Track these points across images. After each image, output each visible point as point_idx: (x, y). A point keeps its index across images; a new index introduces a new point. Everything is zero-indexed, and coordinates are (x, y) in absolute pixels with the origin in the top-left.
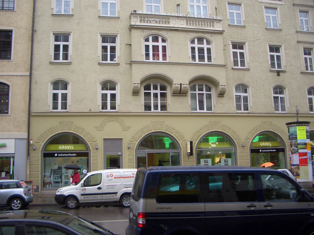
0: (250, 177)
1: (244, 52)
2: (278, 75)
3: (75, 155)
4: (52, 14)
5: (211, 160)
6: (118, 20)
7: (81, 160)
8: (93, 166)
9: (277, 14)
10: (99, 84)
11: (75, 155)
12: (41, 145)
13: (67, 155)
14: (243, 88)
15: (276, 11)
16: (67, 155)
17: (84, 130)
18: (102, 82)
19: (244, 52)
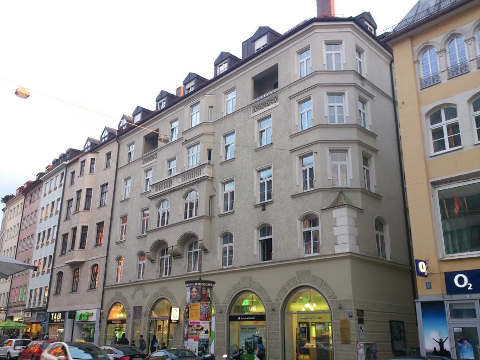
0: (154, 346)
1: (441, 122)
2: (264, 210)
3: (254, 318)
4: (221, 163)
5: (233, 322)
6: (272, 147)
7: (362, 311)
8: (278, 330)
9: (345, 102)
10: (256, 231)
11: (254, 318)
12: (280, 303)
13: (247, 318)
14: (227, 237)
15: (343, 98)
16: (247, 318)
17: (295, 279)
18: (260, 226)
19: (441, 122)
